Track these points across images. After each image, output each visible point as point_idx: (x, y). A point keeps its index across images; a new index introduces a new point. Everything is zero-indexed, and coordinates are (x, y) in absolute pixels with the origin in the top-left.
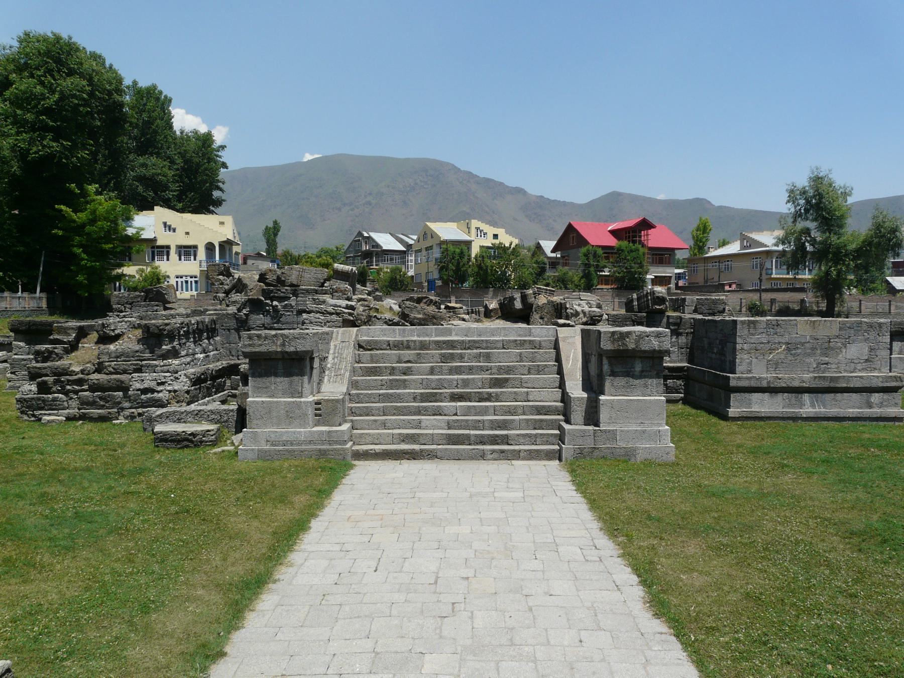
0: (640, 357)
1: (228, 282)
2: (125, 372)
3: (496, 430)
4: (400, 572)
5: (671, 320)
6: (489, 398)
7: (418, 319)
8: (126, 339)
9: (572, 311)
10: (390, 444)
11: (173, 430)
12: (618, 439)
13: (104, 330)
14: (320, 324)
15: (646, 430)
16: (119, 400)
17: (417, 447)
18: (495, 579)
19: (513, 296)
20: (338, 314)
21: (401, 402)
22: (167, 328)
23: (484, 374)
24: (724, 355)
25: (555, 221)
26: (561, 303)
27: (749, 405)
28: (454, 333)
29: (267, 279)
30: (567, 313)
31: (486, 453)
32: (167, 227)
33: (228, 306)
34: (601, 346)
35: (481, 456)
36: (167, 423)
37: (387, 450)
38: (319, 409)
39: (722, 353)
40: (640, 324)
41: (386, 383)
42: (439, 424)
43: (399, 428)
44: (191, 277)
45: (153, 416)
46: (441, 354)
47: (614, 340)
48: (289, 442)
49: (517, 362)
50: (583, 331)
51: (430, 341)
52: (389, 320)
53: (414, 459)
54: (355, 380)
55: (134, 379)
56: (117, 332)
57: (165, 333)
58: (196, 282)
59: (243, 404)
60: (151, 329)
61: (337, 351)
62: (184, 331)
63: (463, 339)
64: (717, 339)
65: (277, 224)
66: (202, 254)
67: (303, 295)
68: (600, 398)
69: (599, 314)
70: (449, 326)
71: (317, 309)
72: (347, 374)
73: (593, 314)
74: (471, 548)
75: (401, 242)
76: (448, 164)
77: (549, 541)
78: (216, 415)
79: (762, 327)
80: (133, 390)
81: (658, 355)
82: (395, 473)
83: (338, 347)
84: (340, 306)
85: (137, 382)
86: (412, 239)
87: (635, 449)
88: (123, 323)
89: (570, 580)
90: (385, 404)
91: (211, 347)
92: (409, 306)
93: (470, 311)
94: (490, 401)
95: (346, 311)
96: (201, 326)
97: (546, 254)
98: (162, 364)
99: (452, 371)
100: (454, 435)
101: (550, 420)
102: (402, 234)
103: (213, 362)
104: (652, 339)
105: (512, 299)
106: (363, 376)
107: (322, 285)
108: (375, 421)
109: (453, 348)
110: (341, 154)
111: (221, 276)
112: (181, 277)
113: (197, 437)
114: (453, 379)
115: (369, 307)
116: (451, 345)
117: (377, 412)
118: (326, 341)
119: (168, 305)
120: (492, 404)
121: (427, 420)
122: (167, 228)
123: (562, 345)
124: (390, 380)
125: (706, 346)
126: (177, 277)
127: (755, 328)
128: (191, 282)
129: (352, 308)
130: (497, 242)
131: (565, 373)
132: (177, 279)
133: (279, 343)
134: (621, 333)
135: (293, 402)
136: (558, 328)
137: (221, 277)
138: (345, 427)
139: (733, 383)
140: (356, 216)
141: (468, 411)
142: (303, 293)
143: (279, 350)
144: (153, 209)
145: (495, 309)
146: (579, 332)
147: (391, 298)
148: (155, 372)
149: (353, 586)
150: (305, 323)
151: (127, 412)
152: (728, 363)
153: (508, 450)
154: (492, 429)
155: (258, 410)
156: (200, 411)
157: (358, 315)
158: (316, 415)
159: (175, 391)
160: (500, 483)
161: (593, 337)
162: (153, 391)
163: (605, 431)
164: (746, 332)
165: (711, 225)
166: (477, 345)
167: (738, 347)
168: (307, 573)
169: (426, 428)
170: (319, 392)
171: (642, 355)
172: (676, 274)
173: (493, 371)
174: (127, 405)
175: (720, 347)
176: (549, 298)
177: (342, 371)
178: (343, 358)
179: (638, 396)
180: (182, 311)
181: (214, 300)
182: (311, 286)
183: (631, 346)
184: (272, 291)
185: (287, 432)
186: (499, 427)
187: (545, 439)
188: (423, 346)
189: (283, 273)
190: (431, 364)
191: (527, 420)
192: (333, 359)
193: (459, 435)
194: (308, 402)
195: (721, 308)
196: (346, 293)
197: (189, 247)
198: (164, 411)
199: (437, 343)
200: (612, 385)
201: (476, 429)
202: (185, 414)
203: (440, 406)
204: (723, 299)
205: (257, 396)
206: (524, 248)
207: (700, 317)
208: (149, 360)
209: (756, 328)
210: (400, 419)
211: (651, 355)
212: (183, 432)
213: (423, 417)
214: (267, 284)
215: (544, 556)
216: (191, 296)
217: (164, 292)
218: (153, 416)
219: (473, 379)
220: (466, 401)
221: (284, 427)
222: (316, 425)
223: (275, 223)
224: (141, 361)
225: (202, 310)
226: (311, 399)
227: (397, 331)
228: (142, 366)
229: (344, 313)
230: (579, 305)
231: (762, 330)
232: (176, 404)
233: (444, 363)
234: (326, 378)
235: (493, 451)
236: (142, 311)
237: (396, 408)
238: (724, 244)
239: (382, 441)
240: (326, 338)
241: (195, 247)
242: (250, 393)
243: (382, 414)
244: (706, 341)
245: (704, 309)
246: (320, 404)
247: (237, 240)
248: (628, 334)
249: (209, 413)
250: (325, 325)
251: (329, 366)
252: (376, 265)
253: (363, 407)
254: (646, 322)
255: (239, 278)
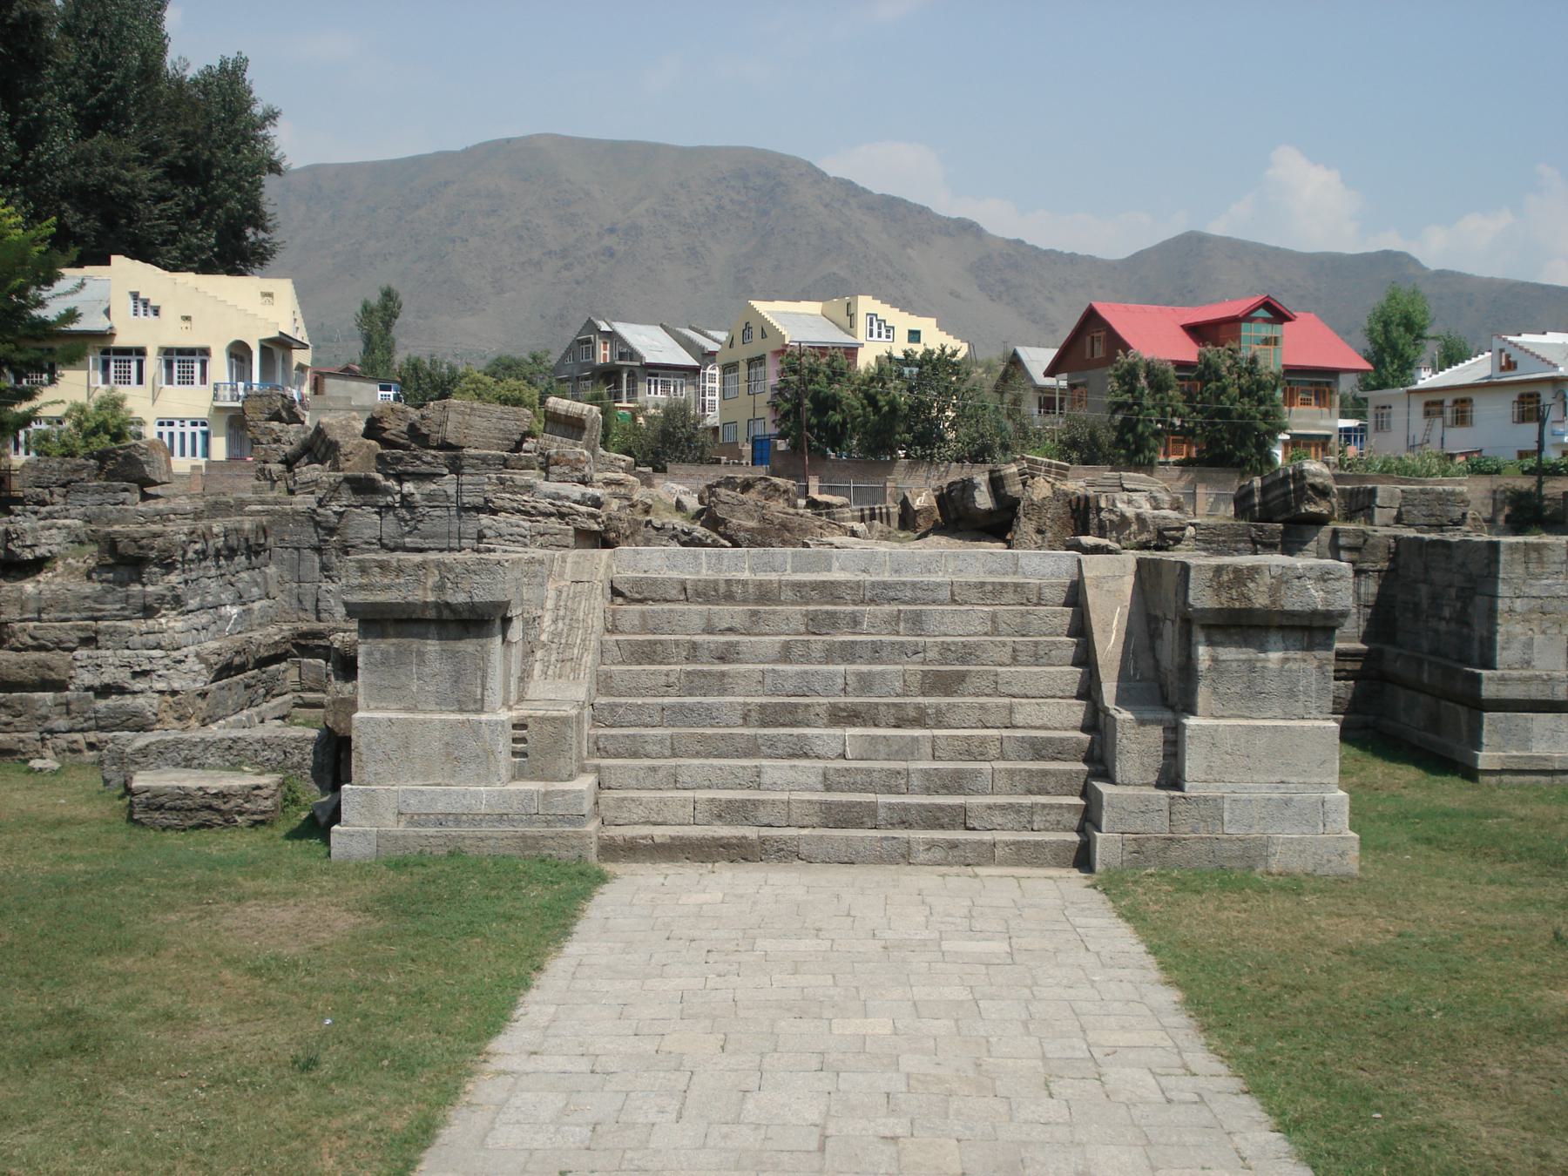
0: (1281, 628)
1: (293, 435)
2: (59, 646)
3: (937, 793)
4: (737, 1121)
5: (1342, 541)
6: (919, 720)
7: (747, 530)
8: (60, 569)
9: (1113, 517)
10: (689, 824)
11: (175, 783)
12: (1226, 818)
13: (10, 545)
14: (520, 540)
15: (1291, 799)
16: (44, 711)
17: (751, 832)
18: (958, 1141)
19: (970, 480)
20: (562, 516)
21: (712, 726)
22: (159, 542)
23: (907, 663)
24: (1468, 625)
25: (1051, 300)
26: (1087, 498)
27: (1525, 742)
28: (836, 565)
29: (385, 430)
30: (1100, 520)
31: (914, 846)
32: (142, 304)
33: (291, 492)
34: (1191, 600)
35: (903, 856)
36: (159, 767)
37: (681, 838)
38: (523, 740)
39: (1463, 619)
40: (1270, 547)
41: (679, 679)
42: (803, 779)
43: (709, 787)
44: (194, 424)
45: (128, 750)
46: (806, 614)
47: (1220, 585)
48: (451, 817)
49: (986, 634)
50: (1140, 563)
51: (780, 581)
52: (683, 531)
53: (746, 860)
54: (606, 673)
55: (78, 664)
56: (39, 551)
57: (153, 554)
58: (206, 435)
59: (338, 725)
60: (121, 546)
61: (562, 603)
62: (196, 552)
63: (858, 579)
64: (1450, 586)
65: (391, 300)
66: (219, 368)
67: (473, 471)
68: (1185, 721)
69: (1176, 525)
70: (821, 548)
71: (515, 505)
72: (588, 659)
73: (1162, 523)
74: (898, 1070)
75: (688, 345)
76: (796, 161)
77: (1079, 1054)
78: (273, 750)
79: (1556, 559)
80: (77, 689)
81: (1322, 623)
82: (704, 891)
83: (564, 594)
84: (567, 498)
85: (85, 669)
86: (715, 340)
87: (1266, 844)
88: (54, 531)
89: (1136, 1145)
90: (676, 730)
91: (255, 590)
92: (726, 499)
93: (867, 512)
94: (924, 726)
95: (583, 509)
96: (233, 541)
97: (1031, 379)
98: (144, 628)
99: (830, 655)
100: (840, 804)
101: (1065, 772)
102: (691, 328)
103: (260, 625)
104: (1309, 584)
105: (968, 486)
106: (623, 662)
107: (518, 447)
108: (654, 769)
109: (836, 599)
110: (539, 136)
111: (276, 423)
112: (171, 424)
113: (232, 803)
114: (833, 675)
115: (629, 499)
116: (829, 591)
117: (657, 748)
118: (539, 579)
119: (150, 490)
120: (927, 732)
121: (774, 767)
122: (141, 309)
123: (1092, 595)
124: (688, 673)
125: (1425, 603)
126: (161, 424)
127: (1540, 561)
128: (194, 435)
129: (597, 503)
130: (919, 349)
131: (1100, 662)
132: (161, 429)
133: (430, 583)
134: (1237, 570)
135: (463, 723)
136: (1083, 557)
137: (275, 425)
138: (585, 783)
139: (1488, 691)
140: (578, 283)
141: (871, 748)
142: (473, 466)
143: (431, 598)
144: (108, 263)
145: (926, 509)
146: (1132, 566)
147: (672, 481)
148: (128, 648)
149: (629, 1155)
150: (485, 537)
151: (62, 741)
152: (1476, 645)
153: (967, 843)
154: (928, 791)
155: (378, 741)
156: (234, 741)
157: (609, 519)
158: (515, 754)
159: (174, 693)
160: (950, 919)
161: (1169, 581)
162: (122, 691)
163: (1197, 800)
164: (1520, 570)
165: (394, 286)
166: (892, 594)
167: (1502, 605)
168: (518, 1122)
169: (773, 787)
170: (521, 700)
171: (1285, 622)
172: (1341, 430)
173: (931, 655)
174: (61, 723)
175: (1459, 605)
176: (1058, 484)
177: (576, 651)
178: (578, 621)
179: (1275, 718)
180: (184, 504)
181: (258, 479)
182: (489, 449)
183: (1260, 601)
184: (399, 460)
185: (445, 794)
186: (945, 787)
187: (1052, 818)
188: (765, 594)
189: (423, 417)
190: (784, 638)
191: (1011, 773)
192: (555, 621)
193: (851, 805)
194: (497, 723)
195: (1456, 513)
196: (580, 466)
197: (191, 352)
198: (153, 740)
199: (798, 586)
200: (1215, 691)
201: (890, 790)
202: (201, 746)
203: (805, 735)
204: (1461, 493)
205: (377, 708)
206: (978, 365)
207: (1411, 533)
208: (115, 618)
209: (1543, 563)
210: (711, 766)
211: (1306, 623)
212: (200, 789)
213: (765, 762)
214: (387, 444)
215: (1069, 1091)
216: (193, 467)
217: (142, 458)
218: (128, 750)
219: (883, 674)
220: (865, 726)
221: (440, 781)
222: (514, 778)
223: (388, 295)
224: (96, 619)
225: (232, 502)
226: (504, 715)
227: (703, 557)
228: (97, 632)
229: (578, 513)
230: (1130, 502)
231: (1556, 568)
232: (176, 724)
233: (814, 634)
234: (538, 667)
235: (931, 845)
236: (90, 503)
237: (703, 739)
238: (1451, 358)
239: (670, 817)
240: (536, 572)
241: (205, 352)
242: (361, 701)
243: (667, 752)
244: (1424, 589)
245: (1417, 514)
246: (524, 726)
247: (301, 335)
248: (1254, 570)
249: (257, 746)
250: (533, 540)
251: (544, 638)
252: (629, 402)
253: (623, 736)
254: (1282, 542)
255: (317, 428)
